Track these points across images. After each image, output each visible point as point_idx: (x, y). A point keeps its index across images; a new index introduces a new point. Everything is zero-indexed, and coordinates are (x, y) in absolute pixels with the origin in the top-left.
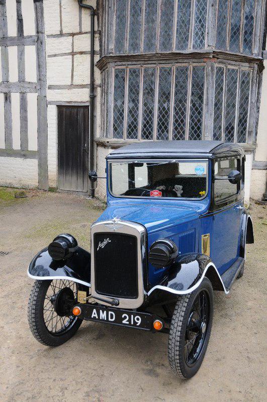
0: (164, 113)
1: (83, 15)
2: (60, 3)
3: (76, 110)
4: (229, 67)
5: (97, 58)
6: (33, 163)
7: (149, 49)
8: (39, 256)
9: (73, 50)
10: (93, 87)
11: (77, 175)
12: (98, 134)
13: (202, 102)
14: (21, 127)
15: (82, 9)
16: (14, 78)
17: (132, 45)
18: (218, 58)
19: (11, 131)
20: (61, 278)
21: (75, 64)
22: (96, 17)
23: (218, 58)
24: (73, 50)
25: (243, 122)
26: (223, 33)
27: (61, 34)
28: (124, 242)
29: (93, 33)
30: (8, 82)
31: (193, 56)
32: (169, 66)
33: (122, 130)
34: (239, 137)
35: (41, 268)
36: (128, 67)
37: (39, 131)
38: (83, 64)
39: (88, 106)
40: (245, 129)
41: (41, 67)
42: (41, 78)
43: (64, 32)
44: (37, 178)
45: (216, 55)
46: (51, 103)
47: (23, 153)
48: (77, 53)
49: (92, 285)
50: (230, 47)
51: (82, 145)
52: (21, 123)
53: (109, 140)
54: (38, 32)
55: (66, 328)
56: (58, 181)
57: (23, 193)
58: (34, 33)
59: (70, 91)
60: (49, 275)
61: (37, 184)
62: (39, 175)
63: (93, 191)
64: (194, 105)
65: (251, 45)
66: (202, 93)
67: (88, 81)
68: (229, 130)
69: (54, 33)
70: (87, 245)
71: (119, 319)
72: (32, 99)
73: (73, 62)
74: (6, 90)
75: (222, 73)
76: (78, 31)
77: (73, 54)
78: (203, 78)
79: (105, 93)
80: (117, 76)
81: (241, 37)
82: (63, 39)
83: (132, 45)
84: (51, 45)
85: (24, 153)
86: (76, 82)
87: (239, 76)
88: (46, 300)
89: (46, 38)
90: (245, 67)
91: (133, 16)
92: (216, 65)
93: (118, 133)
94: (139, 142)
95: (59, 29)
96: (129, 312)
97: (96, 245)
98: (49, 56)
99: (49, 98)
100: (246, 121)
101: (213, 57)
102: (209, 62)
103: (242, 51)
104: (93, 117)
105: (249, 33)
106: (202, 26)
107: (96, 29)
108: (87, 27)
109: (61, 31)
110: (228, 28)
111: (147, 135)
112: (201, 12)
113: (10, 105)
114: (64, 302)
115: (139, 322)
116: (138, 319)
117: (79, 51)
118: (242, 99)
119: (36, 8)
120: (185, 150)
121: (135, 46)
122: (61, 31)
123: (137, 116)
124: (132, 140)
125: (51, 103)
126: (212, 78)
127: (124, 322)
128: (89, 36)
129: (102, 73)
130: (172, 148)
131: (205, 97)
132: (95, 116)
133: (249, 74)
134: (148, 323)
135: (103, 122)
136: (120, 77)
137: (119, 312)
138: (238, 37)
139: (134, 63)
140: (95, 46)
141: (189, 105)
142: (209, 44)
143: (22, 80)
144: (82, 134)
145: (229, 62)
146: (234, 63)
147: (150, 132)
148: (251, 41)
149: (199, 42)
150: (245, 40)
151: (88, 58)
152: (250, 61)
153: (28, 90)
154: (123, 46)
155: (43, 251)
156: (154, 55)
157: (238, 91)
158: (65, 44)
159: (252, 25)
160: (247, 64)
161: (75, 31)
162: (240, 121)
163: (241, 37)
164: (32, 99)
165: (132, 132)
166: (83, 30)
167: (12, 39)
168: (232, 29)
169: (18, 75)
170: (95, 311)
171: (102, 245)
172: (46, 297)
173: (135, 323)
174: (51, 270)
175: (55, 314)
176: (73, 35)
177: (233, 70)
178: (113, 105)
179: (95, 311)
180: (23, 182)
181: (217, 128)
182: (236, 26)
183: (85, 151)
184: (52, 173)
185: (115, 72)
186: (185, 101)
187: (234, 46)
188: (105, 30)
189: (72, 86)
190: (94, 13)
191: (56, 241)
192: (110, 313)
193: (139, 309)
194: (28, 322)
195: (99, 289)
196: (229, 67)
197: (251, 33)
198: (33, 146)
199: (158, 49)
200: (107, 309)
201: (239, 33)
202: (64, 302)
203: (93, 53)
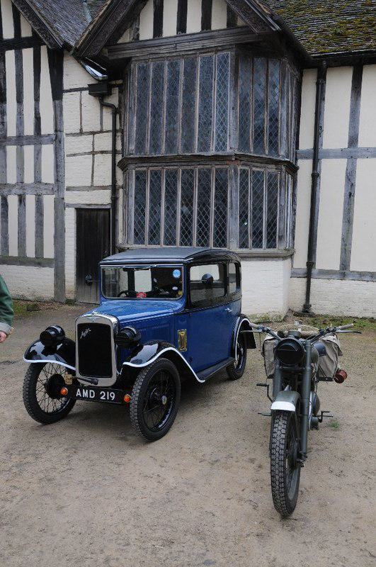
1: (104, 114)
4: (254, 169)
5: (119, 158)
6: (48, 273)
7: (155, 151)
8: (33, 345)
10: (114, 188)
13: (226, 205)
14: (37, 232)
16: (29, 178)
17: (153, 146)
18: (241, 161)
19: (25, 236)
20: (54, 364)
22: (118, 116)
24: (94, 148)
25: (272, 225)
27: (81, 133)
28: (101, 329)
29: (115, 131)
30: (22, 183)
31: (215, 158)
32: (192, 167)
33: (143, 235)
34: (268, 241)
35: (34, 353)
36: (149, 169)
37: (55, 237)
38: (105, 163)
40: (275, 233)
41: (58, 166)
42: (59, 179)
43: (84, 131)
44: (53, 288)
45: (238, 158)
46: (69, 206)
47: (37, 261)
48: (97, 153)
49: (76, 369)
50: (254, 148)
52: (36, 228)
53: (129, 246)
54: (56, 131)
55: (57, 410)
56: (76, 292)
57: (36, 305)
58: (52, 131)
60: (41, 359)
61: (53, 296)
62: (56, 286)
64: (218, 209)
65: (278, 146)
66: (226, 196)
67: (109, 182)
68: (257, 235)
70: (72, 334)
71: (98, 396)
72: (49, 201)
73: (93, 161)
74: (21, 192)
75: (247, 176)
76: (96, 135)
77: (93, 153)
78: (226, 180)
79: (126, 194)
80: (137, 178)
81: (266, 138)
82: (83, 138)
83: (153, 146)
84: (70, 145)
85: (39, 261)
86: (96, 184)
87: (265, 178)
88: (38, 383)
90: (272, 169)
91: (154, 117)
92: (239, 168)
93: (139, 239)
96: (106, 389)
97: (79, 334)
99: (66, 201)
100: (275, 225)
101: (236, 159)
102: (232, 165)
103: (266, 154)
104: (115, 220)
105: (274, 134)
107: (118, 127)
108: (108, 125)
109: (81, 130)
110: (251, 130)
111: (170, 240)
113: (25, 208)
114: (54, 386)
115: (113, 397)
116: (112, 395)
118: (269, 202)
119: (55, 107)
120: (158, 257)
121: (155, 147)
122: (81, 130)
124: (154, 246)
125: (69, 206)
126: (236, 181)
127: (102, 398)
128: (110, 134)
129: (123, 174)
130: (161, 254)
131: (229, 200)
133: (276, 176)
134: (120, 397)
135: (124, 229)
136: (140, 178)
137: (98, 390)
138: (263, 139)
139: (155, 164)
140: (116, 145)
141: (213, 208)
142: (232, 147)
143: (38, 181)
145: (254, 164)
146: (259, 165)
148: (276, 142)
150: (270, 142)
151: (109, 157)
152: (277, 163)
153: (44, 192)
155: (37, 342)
156: (175, 157)
157: (265, 193)
158: (85, 143)
159: (277, 127)
160: (273, 166)
161: (95, 130)
163: (266, 138)
164: (49, 201)
165: (154, 238)
166: (104, 129)
167: (28, 137)
168: (256, 131)
169: (33, 175)
170: (79, 390)
171: (84, 334)
172: (39, 379)
173: (110, 398)
174: (43, 356)
175: (47, 396)
176: (93, 133)
177: (259, 172)
179: (79, 390)
180: (38, 294)
181: (243, 233)
182: (259, 128)
184: (70, 284)
187: (259, 147)
188: (126, 129)
189: (92, 187)
191: (48, 331)
192: (91, 391)
193: (113, 387)
194: (25, 409)
195: (81, 371)
196: (254, 169)
197: (276, 135)
198: (49, 252)
199: (180, 150)
200: (89, 388)
201: (263, 135)
202: (54, 386)
203: (114, 152)
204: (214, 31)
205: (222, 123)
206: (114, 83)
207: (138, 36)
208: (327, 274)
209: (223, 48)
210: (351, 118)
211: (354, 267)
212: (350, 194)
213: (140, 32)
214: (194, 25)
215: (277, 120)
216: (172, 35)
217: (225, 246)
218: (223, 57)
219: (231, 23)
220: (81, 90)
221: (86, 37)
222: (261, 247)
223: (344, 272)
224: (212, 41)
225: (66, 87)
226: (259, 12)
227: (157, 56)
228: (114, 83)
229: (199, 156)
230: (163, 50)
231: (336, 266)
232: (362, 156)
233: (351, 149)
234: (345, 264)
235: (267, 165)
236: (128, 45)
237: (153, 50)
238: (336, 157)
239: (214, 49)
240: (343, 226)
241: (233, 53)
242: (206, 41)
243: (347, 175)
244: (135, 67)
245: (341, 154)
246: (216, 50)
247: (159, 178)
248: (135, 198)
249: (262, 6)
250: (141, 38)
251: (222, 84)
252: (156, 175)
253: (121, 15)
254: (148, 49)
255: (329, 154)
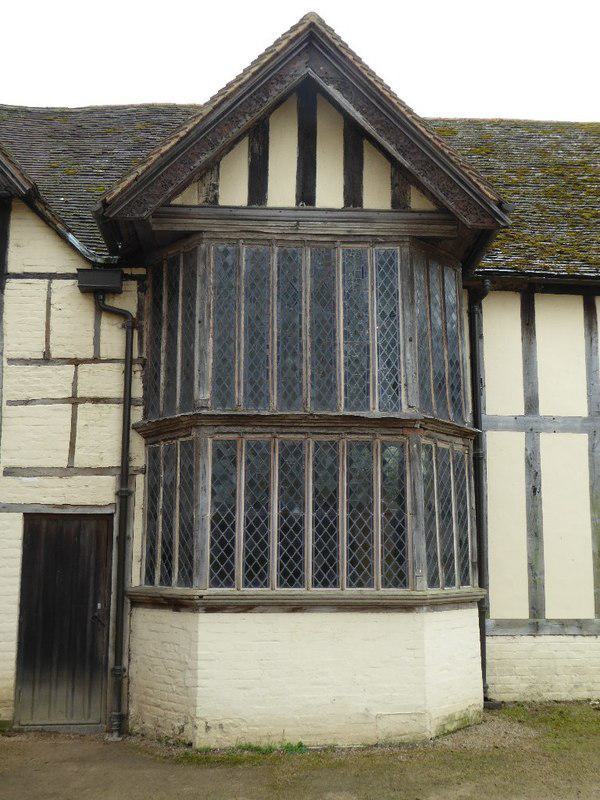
0: (291, 530)
2: (49, 299)
3: (76, 523)
7: (257, 404)
9: (75, 391)
10: (125, 474)
11: (73, 681)
12: (136, 578)
13: (404, 508)
15: (103, 314)
17: (252, 395)
18: (425, 429)
21: (80, 423)
22: (136, 333)
23: (425, 429)
24: (75, 391)
26: (426, 386)
27: (47, 359)
32: (334, 438)
36: (245, 438)
39: (112, 515)
43: (54, 355)
45: (431, 425)
48: (84, 400)
51: (91, 605)
53: (201, 592)
59: (65, 482)
63: (123, 718)
67: (113, 459)
69: (28, 356)
76: (90, 355)
77: (75, 401)
80: (218, 454)
82: (47, 369)
86: (79, 462)
89: (5, 364)
92: (424, 441)
94: (238, 593)
95: (43, 347)
98: (10, 403)
104: (124, 540)
106: (394, 371)
107: (136, 355)
112: (389, 348)
117: (92, 396)
123: (267, 538)
132: (129, 538)
144: (92, 579)
146: (445, 437)
147: (228, 564)
149: (390, 397)
150: (453, 399)
151: (115, 413)
154: (230, 395)
156: (305, 417)
159: (458, 376)
160: (459, 441)
161: (81, 356)
162: (250, 529)
176: (76, 362)
178: (209, 515)
183: (100, 621)
185: (214, 446)
186: (371, 507)
189: (70, 470)
190: (133, 324)
196: (441, 445)
203: (127, 402)
204: (319, 210)
205: (392, 365)
206: (127, 271)
207: (216, 198)
208: (509, 626)
209: (386, 240)
210: (524, 370)
211: (551, 612)
212: (535, 490)
213: (221, 191)
214: (330, 192)
215: (458, 364)
216: (286, 205)
217: (405, 585)
218: (386, 253)
219: (399, 203)
220: (51, 276)
221: (129, 185)
222: (301, 584)
223: (536, 622)
224: (367, 225)
225: (12, 268)
226: (474, 193)
227: (255, 236)
228: (127, 271)
229: (345, 416)
230: (272, 229)
231: (523, 612)
232: (547, 430)
233: (530, 418)
234: (537, 606)
235: (454, 439)
236: (193, 210)
237: (249, 225)
238: (506, 428)
239: (369, 239)
240: (529, 542)
241: (406, 250)
242: (358, 225)
243: (527, 459)
244: (209, 250)
245: (516, 424)
246: (375, 240)
247: (267, 457)
248: (213, 493)
249: (482, 187)
250: (221, 202)
251: (387, 293)
252: (258, 453)
253: (203, 158)
254: (241, 223)
255: (499, 424)
